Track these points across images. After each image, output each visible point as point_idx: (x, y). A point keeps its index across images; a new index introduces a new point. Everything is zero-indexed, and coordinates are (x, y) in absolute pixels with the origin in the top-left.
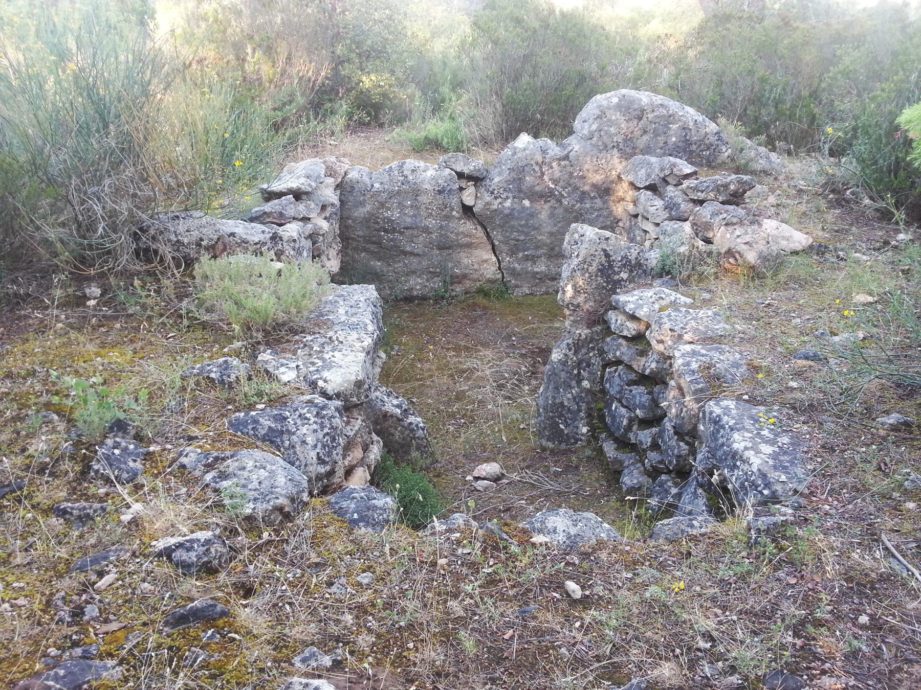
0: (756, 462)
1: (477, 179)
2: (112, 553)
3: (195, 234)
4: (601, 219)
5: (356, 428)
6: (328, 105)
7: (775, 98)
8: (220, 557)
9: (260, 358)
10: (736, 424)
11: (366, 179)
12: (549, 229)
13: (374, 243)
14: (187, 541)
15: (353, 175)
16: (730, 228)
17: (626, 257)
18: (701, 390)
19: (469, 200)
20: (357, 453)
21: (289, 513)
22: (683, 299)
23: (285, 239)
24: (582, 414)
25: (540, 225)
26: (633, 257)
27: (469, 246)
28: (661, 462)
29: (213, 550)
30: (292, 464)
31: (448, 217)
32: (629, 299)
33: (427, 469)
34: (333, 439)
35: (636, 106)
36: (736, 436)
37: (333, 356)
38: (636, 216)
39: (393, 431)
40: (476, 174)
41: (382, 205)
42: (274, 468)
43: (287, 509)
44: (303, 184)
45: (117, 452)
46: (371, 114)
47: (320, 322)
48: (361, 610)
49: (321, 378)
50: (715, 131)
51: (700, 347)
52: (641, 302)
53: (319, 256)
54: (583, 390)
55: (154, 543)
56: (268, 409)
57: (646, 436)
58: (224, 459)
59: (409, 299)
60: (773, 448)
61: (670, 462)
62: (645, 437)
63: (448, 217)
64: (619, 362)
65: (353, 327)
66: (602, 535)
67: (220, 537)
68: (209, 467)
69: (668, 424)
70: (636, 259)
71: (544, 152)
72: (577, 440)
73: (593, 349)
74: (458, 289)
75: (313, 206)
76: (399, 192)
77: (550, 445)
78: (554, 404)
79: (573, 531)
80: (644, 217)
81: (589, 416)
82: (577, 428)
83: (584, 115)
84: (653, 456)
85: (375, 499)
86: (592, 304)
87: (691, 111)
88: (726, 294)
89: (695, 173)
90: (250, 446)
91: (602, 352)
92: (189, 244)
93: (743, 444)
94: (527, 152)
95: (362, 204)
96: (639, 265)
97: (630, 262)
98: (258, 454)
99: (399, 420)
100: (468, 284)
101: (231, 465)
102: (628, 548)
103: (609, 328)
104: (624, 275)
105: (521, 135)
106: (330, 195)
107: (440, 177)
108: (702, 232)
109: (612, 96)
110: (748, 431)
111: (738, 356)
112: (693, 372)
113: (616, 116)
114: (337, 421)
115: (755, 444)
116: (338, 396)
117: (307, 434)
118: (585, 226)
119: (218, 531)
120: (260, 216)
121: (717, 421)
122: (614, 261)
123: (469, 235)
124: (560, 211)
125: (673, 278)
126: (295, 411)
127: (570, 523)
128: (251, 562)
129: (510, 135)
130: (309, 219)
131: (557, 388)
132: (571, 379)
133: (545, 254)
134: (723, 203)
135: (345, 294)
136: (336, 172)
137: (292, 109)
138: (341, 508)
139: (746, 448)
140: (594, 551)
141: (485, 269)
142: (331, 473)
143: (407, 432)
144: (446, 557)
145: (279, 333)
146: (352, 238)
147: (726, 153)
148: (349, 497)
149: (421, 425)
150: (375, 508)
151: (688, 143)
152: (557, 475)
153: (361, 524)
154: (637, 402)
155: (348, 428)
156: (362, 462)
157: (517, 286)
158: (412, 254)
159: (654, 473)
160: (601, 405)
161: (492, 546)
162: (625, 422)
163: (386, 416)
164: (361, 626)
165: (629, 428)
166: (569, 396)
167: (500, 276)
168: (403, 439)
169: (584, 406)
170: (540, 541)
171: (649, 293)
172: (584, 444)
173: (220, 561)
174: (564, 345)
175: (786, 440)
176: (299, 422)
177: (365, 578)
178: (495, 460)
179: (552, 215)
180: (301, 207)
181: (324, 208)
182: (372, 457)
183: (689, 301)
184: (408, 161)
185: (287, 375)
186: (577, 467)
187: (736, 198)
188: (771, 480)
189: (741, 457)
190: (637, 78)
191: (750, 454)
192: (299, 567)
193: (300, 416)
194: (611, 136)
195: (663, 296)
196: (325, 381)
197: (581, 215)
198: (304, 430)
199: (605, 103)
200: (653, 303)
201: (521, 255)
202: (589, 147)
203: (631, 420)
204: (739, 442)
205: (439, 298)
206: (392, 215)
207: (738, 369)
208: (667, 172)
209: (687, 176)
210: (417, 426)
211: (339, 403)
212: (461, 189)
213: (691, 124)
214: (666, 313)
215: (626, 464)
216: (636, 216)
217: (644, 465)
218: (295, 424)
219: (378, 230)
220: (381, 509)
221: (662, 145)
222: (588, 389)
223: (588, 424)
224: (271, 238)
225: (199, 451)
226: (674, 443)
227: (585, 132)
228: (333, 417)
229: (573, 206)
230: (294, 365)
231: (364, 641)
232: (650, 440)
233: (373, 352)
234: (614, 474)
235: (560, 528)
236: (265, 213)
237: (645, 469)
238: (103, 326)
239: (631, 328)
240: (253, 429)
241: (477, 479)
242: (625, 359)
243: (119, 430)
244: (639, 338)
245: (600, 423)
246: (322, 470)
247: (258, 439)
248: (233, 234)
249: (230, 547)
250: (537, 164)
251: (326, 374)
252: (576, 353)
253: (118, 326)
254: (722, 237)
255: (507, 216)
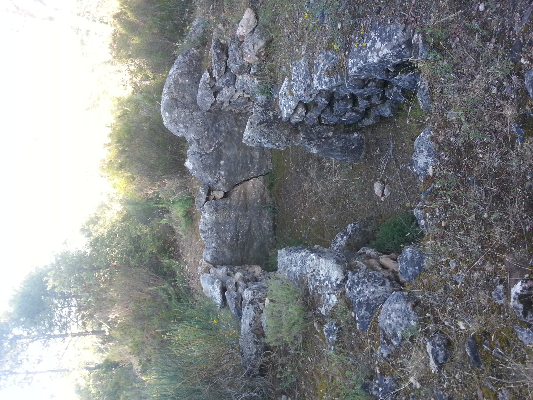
0: (385, 51)
1: (210, 190)
2: (439, 393)
3: (251, 345)
4: (231, 121)
5: (362, 263)
6: (165, 269)
7: (160, 21)
8: (442, 339)
9: (324, 314)
10: (363, 60)
11: (210, 251)
12: (236, 150)
13: (244, 246)
14: (433, 355)
15: (208, 258)
16: (245, 55)
17: (261, 113)
18: (341, 76)
19: (221, 194)
20: (373, 261)
21: (415, 302)
22: (285, 82)
23: (253, 297)
24: (347, 136)
25: (234, 155)
26: (261, 109)
27: (245, 194)
28: (378, 95)
29: (438, 342)
30: (385, 300)
31: (230, 206)
32: (285, 112)
33: (377, 222)
34: (371, 277)
35: (170, 102)
36: (370, 60)
37: (322, 275)
38: (230, 102)
39: (356, 241)
40: (207, 191)
41: (224, 242)
42: (390, 309)
43: (414, 304)
44: (218, 286)
45: (380, 389)
46: (168, 246)
47: (301, 280)
48: (472, 269)
49: (336, 282)
50: (182, 57)
51: (315, 75)
52: (287, 106)
53: (255, 278)
54: (334, 136)
55: (433, 372)
56: (355, 310)
57: (363, 103)
58: (385, 335)
59: (275, 228)
60: (378, 41)
61: (379, 91)
62: (362, 104)
63: (230, 206)
64: (319, 117)
65: (303, 263)
66: (427, 137)
67: (430, 339)
68: (389, 342)
69: (357, 92)
70: (262, 107)
71: (195, 153)
72: (361, 139)
73: (311, 130)
74: (269, 200)
75: (229, 281)
76: (217, 233)
77: (363, 153)
78: (341, 152)
79: (426, 153)
80: (231, 98)
81: (348, 132)
82: (354, 139)
83: (175, 131)
84: (374, 100)
85: (406, 257)
86: (286, 131)
87: (171, 71)
88: (280, 57)
89: (209, 70)
90: (376, 320)
91: (313, 126)
92: (257, 348)
93: (375, 57)
94: (195, 162)
95: (223, 253)
96: (265, 105)
97: (263, 110)
98: (381, 318)
99: (350, 237)
100: (266, 195)
101: (389, 331)
102: (436, 124)
103: (300, 122)
104: (271, 114)
105: (185, 165)
106: (222, 271)
107: (208, 210)
108: (245, 69)
109: (165, 116)
110: (367, 53)
111: (321, 55)
112: (330, 80)
113: (175, 114)
114: (361, 274)
115: (375, 50)
116: (345, 273)
117: (369, 291)
118: (244, 135)
119: (427, 339)
120: (237, 310)
121: (361, 70)
122: (263, 120)
123: (240, 194)
124: (226, 144)
125: (272, 86)
126: (356, 297)
127: (421, 155)
128: (443, 323)
129: (185, 171)
130: (236, 283)
131: (332, 150)
132: (328, 142)
133: (250, 152)
134: (228, 57)
135: (283, 266)
136: (207, 267)
137: (171, 290)
138: (412, 275)
139: (378, 56)
140: (437, 143)
141: (257, 185)
142: (389, 278)
143: (357, 233)
144: (441, 222)
145: (309, 302)
146: (242, 259)
147: (194, 51)
148: (406, 271)
149: (352, 225)
150: (412, 257)
151: (189, 72)
152: (381, 151)
153: (421, 265)
154: (343, 108)
155: (362, 268)
156: (377, 259)
157: (267, 167)
158: (250, 226)
159: (384, 99)
160: (342, 126)
161: (434, 196)
162: (354, 114)
163: (348, 244)
164: (481, 268)
165: (357, 112)
166: (337, 143)
167: (262, 177)
168: (360, 235)
169: (343, 135)
170: (432, 171)
171: (282, 101)
172: (364, 135)
173: (444, 339)
174: (309, 147)
175: (373, 34)
176: (362, 295)
177: (453, 265)
178: (373, 185)
179: (229, 148)
180: (230, 287)
181: (229, 275)
182: (373, 253)
183: (286, 79)
184: (200, 228)
185: (334, 299)
186: (377, 139)
187: (224, 49)
188: (397, 44)
189: (382, 58)
190: (152, 101)
191: (381, 54)
192: (446, 299)
193: (358, 294)
194: (186, 116)
195: (284, 93)
196: (337, 280)
197: (228, 132)
198: (367, 292)
199: (168, 120)
200: (288, 99)
201: (250, 165)
202: (192, 129)
203: (353, 111)
204: (374, 59)
205: (274, 211)
206: (230, 237)
207: (329, 56)
208: (208, 86)
209: (211, 75)
210: (353, 227)
211: (350, 273)
212: (215, 199)
213: (179, 71)
214: (294, 92)
215: (377, 114)
216: (230, 102)
217: (379, 104)
218: (363, 297)
219: (237, 244)
220: (413, 254)
221: (190, 88)
222: (333, 133)
223: (353, 133)
224: (252, 304)
225: (380, 347)
226: (369, 89)
227: (184, 130)
228: (358, 276)
229: (223, 136)
230: (328, 296)
231: (489, 268)
232: (365, 101)
233: (320, 254)
234: (382, 119)
235: (425, 160)
236: (236, 307)
237: (381, 104)
238: (304, 395)
239: (301, 111)
240: (366, 319)
241: (383, 194)
242: (318, 113)
243: (367, 388)
244: (307, 107)
245: (351, 127)
246: (388, 283)
247: (372, 316)
248: (250, 325)
249: (435, 333)
250: (201, 157)
251: (333, 279)
252: (313, 140)
253: (303, 387)
254: (249, 59)
255: (229, 173)
